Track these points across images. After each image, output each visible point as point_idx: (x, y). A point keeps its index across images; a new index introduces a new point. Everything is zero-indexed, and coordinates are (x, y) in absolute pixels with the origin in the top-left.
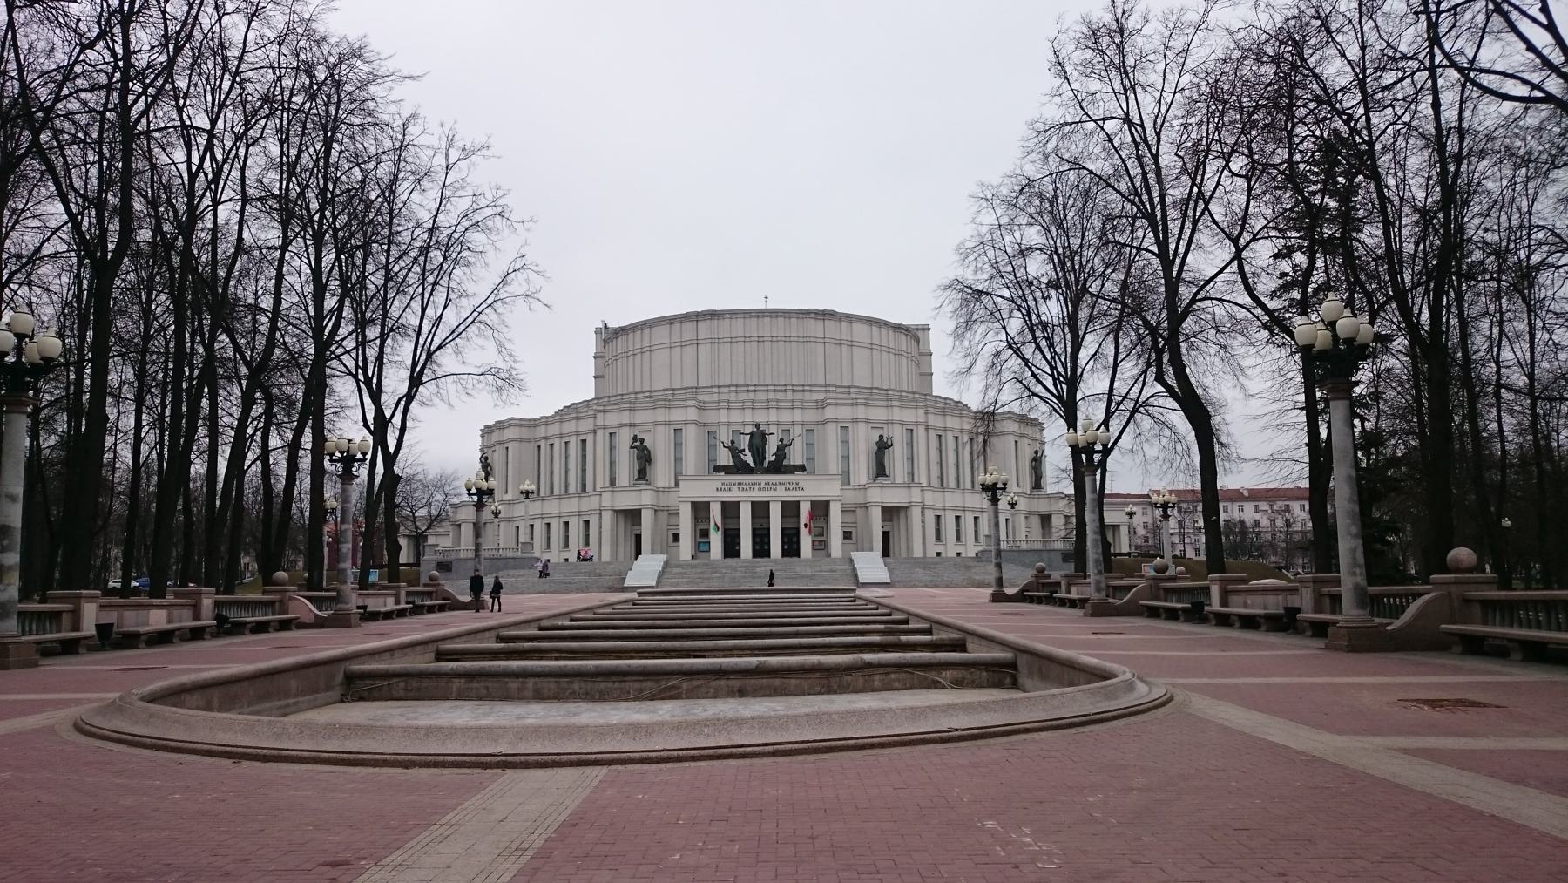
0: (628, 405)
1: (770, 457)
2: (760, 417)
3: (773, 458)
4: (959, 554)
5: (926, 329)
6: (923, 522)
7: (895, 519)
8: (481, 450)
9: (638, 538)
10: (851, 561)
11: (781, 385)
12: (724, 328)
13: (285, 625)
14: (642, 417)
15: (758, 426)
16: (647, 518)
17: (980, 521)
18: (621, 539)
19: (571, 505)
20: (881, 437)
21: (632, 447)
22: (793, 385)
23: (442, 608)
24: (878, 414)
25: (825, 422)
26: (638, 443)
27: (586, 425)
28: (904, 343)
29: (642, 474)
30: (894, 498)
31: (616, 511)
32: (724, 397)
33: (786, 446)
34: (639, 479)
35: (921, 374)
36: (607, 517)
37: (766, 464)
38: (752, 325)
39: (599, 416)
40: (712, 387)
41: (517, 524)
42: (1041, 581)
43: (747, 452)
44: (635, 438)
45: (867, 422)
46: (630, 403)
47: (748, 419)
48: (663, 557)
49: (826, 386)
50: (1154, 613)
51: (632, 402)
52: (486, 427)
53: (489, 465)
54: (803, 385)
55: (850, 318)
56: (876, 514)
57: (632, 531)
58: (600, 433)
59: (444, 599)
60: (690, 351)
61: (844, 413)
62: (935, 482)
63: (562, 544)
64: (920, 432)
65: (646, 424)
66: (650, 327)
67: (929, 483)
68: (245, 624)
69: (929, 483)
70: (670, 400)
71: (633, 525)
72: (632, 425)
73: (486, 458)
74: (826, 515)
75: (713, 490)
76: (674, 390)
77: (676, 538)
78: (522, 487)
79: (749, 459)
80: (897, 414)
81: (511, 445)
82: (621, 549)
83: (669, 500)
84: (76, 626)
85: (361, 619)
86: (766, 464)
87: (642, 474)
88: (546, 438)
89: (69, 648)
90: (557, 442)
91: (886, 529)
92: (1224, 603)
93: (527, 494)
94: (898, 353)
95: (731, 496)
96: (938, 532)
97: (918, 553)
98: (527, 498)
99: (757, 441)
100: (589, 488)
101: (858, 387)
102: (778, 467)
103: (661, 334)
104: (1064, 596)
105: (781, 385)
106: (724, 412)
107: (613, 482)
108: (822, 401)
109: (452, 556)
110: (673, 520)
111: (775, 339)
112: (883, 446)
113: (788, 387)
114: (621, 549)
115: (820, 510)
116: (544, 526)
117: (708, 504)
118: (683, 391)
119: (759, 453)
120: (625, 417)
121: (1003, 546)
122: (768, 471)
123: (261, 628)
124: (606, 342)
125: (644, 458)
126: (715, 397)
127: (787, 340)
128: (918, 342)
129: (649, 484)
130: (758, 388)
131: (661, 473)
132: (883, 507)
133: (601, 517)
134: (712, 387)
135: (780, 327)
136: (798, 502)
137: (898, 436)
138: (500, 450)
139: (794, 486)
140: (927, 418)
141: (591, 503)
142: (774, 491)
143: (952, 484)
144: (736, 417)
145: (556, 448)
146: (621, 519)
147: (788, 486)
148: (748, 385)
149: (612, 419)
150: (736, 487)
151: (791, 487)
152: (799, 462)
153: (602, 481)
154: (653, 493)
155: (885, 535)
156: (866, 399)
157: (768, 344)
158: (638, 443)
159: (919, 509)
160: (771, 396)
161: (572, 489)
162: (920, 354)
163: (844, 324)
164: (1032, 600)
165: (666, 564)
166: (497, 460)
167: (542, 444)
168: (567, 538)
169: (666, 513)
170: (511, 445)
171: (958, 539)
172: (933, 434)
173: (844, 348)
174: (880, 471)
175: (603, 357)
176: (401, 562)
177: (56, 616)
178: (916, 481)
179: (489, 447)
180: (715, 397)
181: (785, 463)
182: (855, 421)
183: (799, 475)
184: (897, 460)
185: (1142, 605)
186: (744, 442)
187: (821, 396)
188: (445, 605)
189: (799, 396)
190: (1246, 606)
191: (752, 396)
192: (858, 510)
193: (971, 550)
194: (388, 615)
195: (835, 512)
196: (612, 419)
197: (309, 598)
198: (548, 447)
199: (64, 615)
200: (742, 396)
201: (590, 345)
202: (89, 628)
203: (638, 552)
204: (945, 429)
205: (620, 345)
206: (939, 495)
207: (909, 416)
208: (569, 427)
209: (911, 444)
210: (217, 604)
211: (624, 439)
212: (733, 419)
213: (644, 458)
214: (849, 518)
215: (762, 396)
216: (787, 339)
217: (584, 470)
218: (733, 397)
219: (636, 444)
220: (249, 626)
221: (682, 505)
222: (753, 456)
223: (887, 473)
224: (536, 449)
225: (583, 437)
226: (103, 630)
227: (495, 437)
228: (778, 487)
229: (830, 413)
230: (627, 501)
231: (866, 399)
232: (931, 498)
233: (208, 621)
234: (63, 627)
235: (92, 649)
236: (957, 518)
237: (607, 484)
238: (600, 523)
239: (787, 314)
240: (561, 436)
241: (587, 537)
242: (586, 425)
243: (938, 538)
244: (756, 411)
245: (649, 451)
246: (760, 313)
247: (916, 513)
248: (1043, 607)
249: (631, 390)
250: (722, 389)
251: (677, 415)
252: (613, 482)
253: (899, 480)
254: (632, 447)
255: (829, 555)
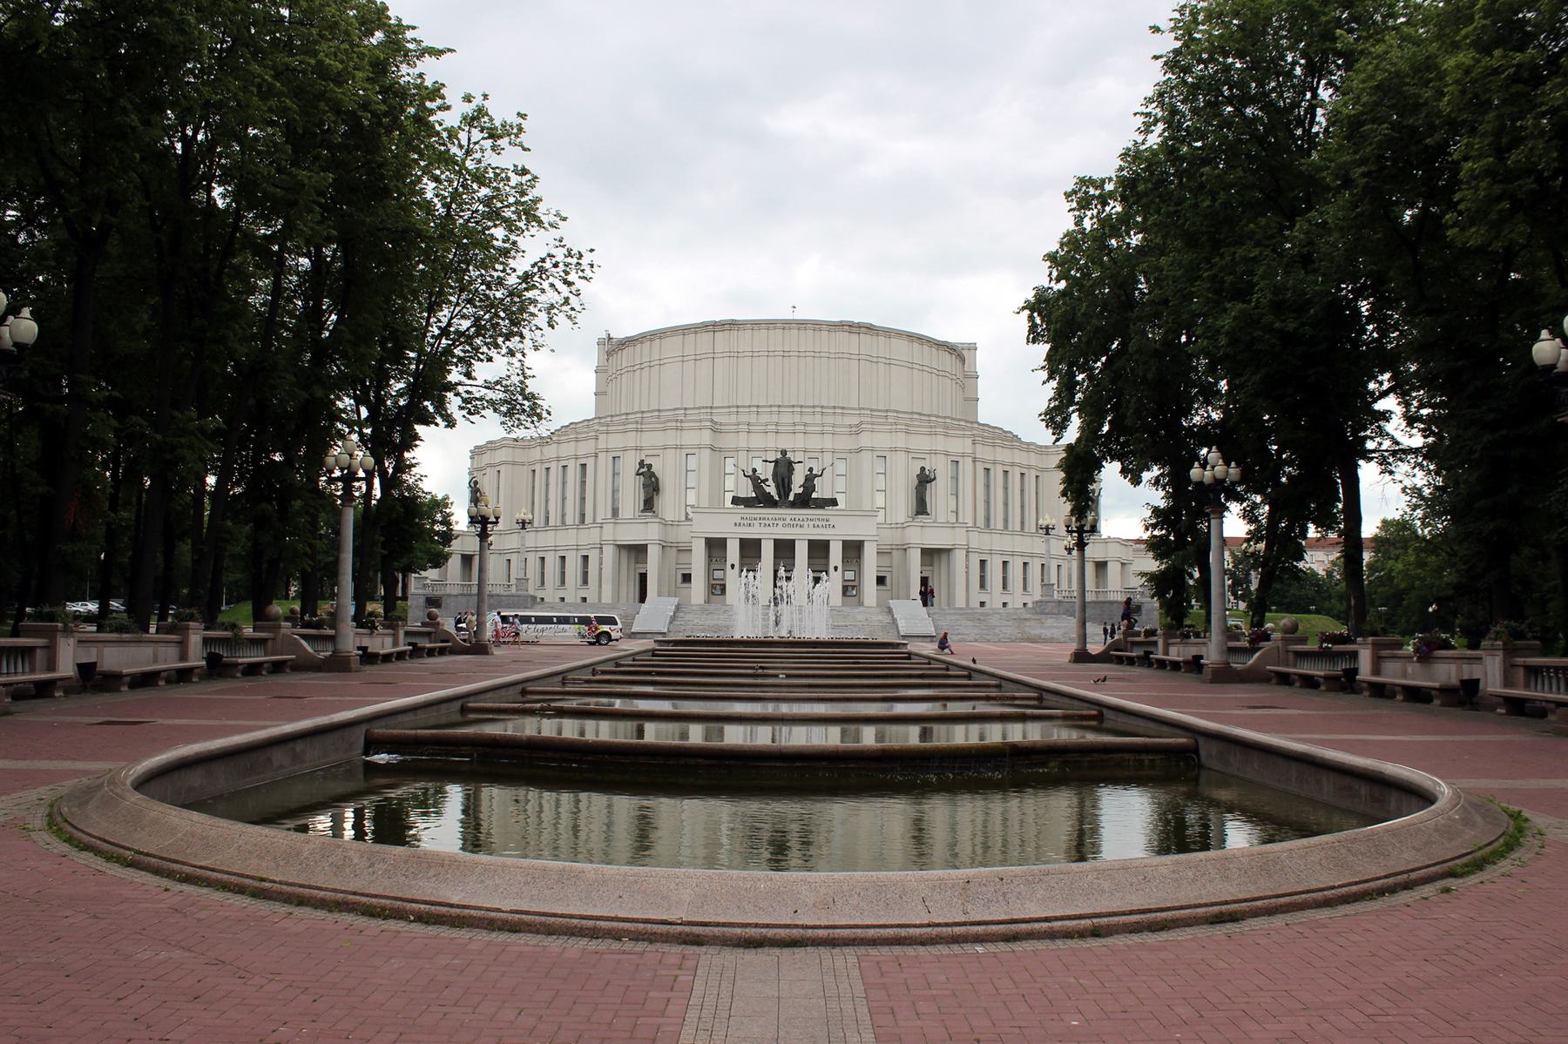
0: (634, 426)
1: (797, 488)
2: (785, 442)
3: (800, 491)
4: (1005, 604)
5: (972, 348)
6: (967, 567)
7: (936, 564)
8: (470, 473)
9: (643, 578)
10: (890, 611)
11: (808, 407)
12: (744, 340)
13: (277, 667)
14: (649, 439)
15: (784, 453)
16: (653, 553)
17: (1010, 566)
18: (624, 573)
19: (567, 538)
20: (923, 469)
21: (638, 474)
22: (822, 407)
23: (442, 652)
24: (921, 443)
25: (859, 450)
26: (645, 469)
27: (586, 448)
28: (947, 361)
29: (649, 505)
30: (936, 539)
31: (620, 547)
32: (744, 418)
33: (816, 476)
34: (918, 513)
35: (966, 399)
36: (609, 552)
37: (791, 498)
38: (776, 339)
39: (602, 437)
40: (729, 407)
41: (508, 557)
42: (1130, 639)
43: (770, 482)
44: (642, 464)
45: (908, 451)
46: (637, 423)
47: (771, 445)
48: (675, 601)
49: (860, 409)
50: (1284, 679)
51: (639, 422)
52: (476, 447)
53: (478, 490)
54: (834, 407)
55: (889, 333)
56: (915, 557)
57: (635, 569)
58: (602, 456)
59: (442, 641)
60: (705, 365)
61: (882, 440)
62: (981, 522)
63: (558, 582)
64: (966, 465)
65: (653, 448)
66: (651, 340)
67: (975, 523)
68: (424, 648)
69: (975, 523)
70: (682, 421)
71: (637, 563)
72: (638, 449)
73: (476, 483)
74: (826, 556)
75: (733, 526)
76: (686, 409)
77: (687, 578)
78: (517, 516)
79: (771, 489)
80: (940, 443)
81: (503, 468)
82: (624, 590)
83: (681, 535)
84: (51, 665)
85: (362, 663)
86: (791, 498)
87: (649, 505)
88: (541, 461)
89: (43, 690)
90: (553, 466)
91: (924, 575)
92: (1376, 670)
93: (523, 524)
94: (941, 373)
95: (751, 533)
96: (982, 578)
97: (960, 602)
98: (523, 528)
99: (782, 470)
100: (588, 519)
101: (897, 412)
102: (804, 501)
103: (672, 347)
104: (1160, 656)
105: (808, 407)
106: (743, 436)
107: (615, 512)
108: (857, 426)
109: (438, 592)
110: (684, 558)
111: (786, 354)
112: (924, 480)
113: (817, 410)
114: (624, 590)
115: (853, 549)
116: (558, 561)
117: (793, 541)
118: (698, 411)
119: (784, 483)
120: (631, 440)
121: (1089, 597)
122: (793, 505)
123: (253, 670)
124: (609, 354)
125: (651, 486)
126: (733, 419)
127: (816, 355)
128: (963, 361)
129: (657, 517)
130: (804, 410)
131: (668, 504)
132: (922, 549)
133: (601, 552)
134: (729, 407)
135: (807, 340)
136: (794, 540)
137: (941, 468)
138: (491, 472)
139: (824, 523)
140: (975, 449)
141: (590, 536)
142: (800, 527)
143: (1000, 525)
144: (757, 441)
145: (553, 472)
146: (624, 554)
147: (817, 523)
148: (771, 406)
149: (616, 441)
150: (756, 523)
151: (820, 523)
152: (827, 496)
153: (604, 512)
154: (662, 526)
155: (924, 581)
156: (907, 425)
157: (794, 360)
158: (645, 469)
159: (964, 552)
160: (797, 418)
161: (569, 520)
162: (966, 377)
163: (881, 339)
164: (1120, 660)
165: (678, 608)
166: (487, 486)
167: (537, 467)
168: (563, 574)
169: (674, 550)
170: (503, 468)
171: (1005, 587)
172: (980, 467)
173: (881, 366)
174: (921, 508)
175: (606, 371)
176: (692, 602)
177: (28, 652)
178: (960, 521)
179: (479, 470)
180: (733, 419)
181: (814, 495)
182: (895, 450)
183: (829, 510)
184: (939, 495)
185: (1271, 671)
186: (766, 472)
187: (855, 421)
188: (445, 648)
189: (829, 420)
190: (1405, 676)
191: (775, 418)
192: (894, 552)
193: (1016, 599)
194: (387, 658)
195: (870, 553)
196: (616, 441)
197: (304, 637)
198: (544, 471)
199: (38, 651)
200: (764, 418)
201: (593, 357)
202: (66, 667)
203: (643, 598)
204: (994, 462)
205: (626, 356)
206: (986, 537)
207: (960, 445)
208: (567, 449)
209: (956, 478)
210: (206, 641)
211: (629, 465)
212: (810, 446)
213: (651, 486)
214: (885, 561)
215: (786, 418)
216: (817, 355)
217: (583, 499)
218: (753, 418)
219: (642, 470)
220: (240, 667)
221: (693, 540)
222: (777, 487)
223: (929, 511)
224: (531, 473)
225: (564, 463)
226: (86, 670)
227: (486, 459)
228: (806, 524)
229: (865, 440)
230: (632, 535)
231: (907, 425)
232: (978, 541)
233: (196, 659)
234: (38, 664)
235: (69, 691)
236: (1005, 563)
237: (609, 516)
238: (601, 559)
239: (817, 325)
240: (558, 459)
241: (585, 574)
242: (586, 448)
243: (982, 586)
244: (836, 436)
245: (657, 479)
246: (786, 325)
247: (959, 557)
248: (1137, 671)
249: (636, 409)
250: (740, 410)
251: (690, 438)
252: (615, 512)
253: (941, 519)
254: (638, 474)
255: (861, 604)
